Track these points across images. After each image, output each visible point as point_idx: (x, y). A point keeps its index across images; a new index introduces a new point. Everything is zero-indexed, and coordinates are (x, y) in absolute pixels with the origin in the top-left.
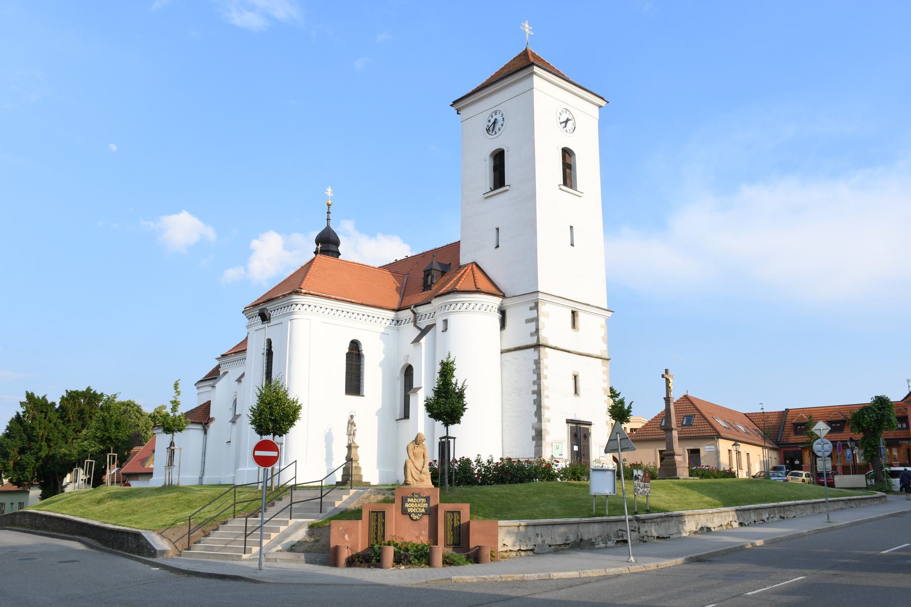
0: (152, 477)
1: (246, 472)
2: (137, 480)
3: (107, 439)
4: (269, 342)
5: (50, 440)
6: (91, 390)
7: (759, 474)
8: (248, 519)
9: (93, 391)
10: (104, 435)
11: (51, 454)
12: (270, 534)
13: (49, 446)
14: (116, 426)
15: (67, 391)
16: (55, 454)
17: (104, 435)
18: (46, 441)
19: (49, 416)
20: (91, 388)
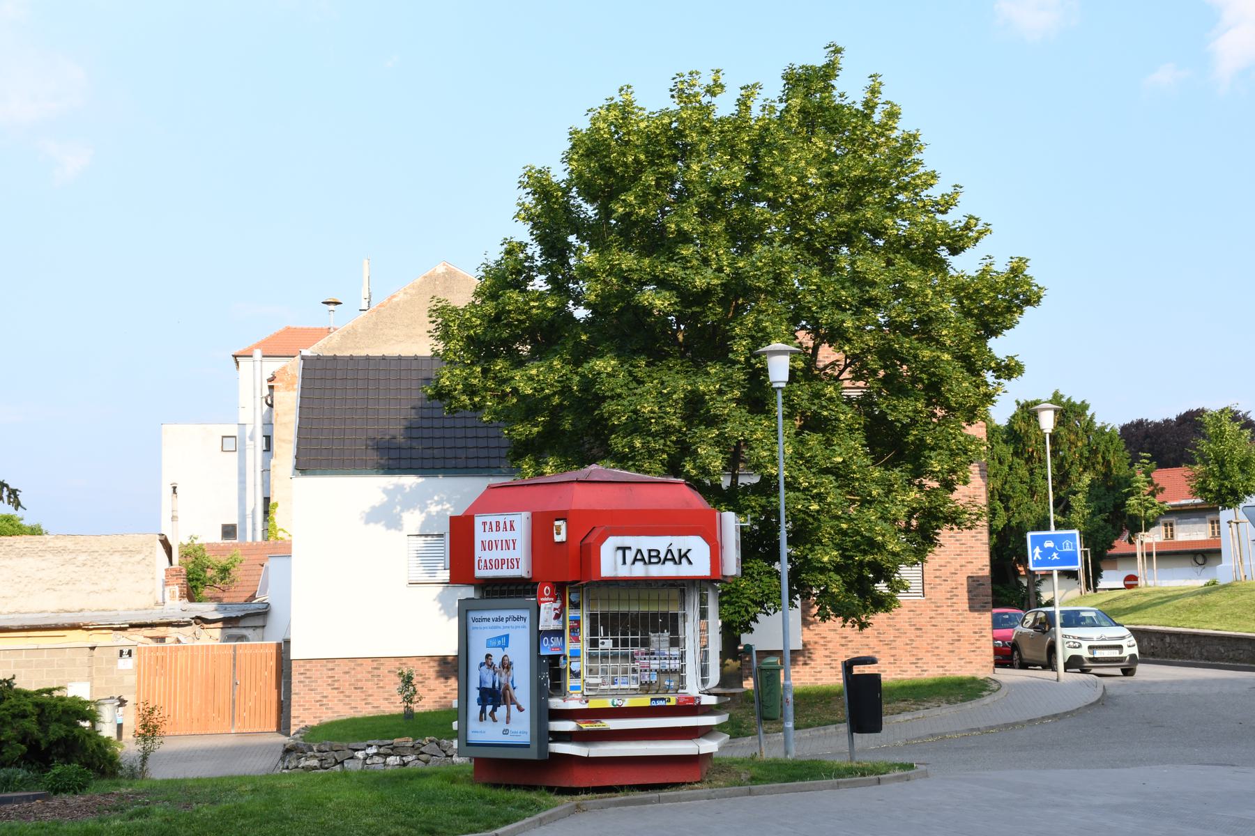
0: (1221, 562)
1: (1154, 545)
2: (1116, 569)
3: (1228, 494)
4: (323, 303)
5: (1008, 498)
6: (1062, 396)
7: (941, 515)
8: (472, 615)
9: (1067, 397)
10: (1222, 485)
11: (1014, 523)
12: (756, 651)
13: (1007, 509)
14: (1240, 468)
15: (1018, 403)
16: (1021, 522)
17: (1222, 485)
18: (1001, 501)
19: (999, 452)
20: (1061, 393)
